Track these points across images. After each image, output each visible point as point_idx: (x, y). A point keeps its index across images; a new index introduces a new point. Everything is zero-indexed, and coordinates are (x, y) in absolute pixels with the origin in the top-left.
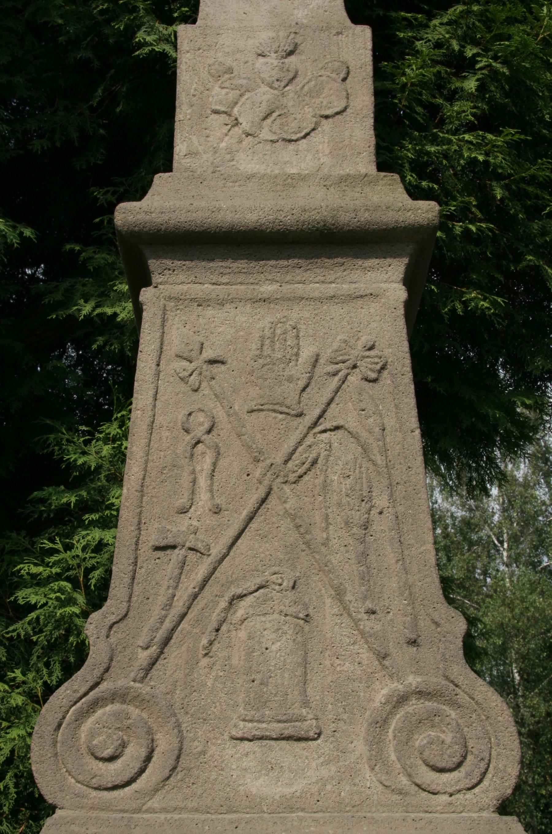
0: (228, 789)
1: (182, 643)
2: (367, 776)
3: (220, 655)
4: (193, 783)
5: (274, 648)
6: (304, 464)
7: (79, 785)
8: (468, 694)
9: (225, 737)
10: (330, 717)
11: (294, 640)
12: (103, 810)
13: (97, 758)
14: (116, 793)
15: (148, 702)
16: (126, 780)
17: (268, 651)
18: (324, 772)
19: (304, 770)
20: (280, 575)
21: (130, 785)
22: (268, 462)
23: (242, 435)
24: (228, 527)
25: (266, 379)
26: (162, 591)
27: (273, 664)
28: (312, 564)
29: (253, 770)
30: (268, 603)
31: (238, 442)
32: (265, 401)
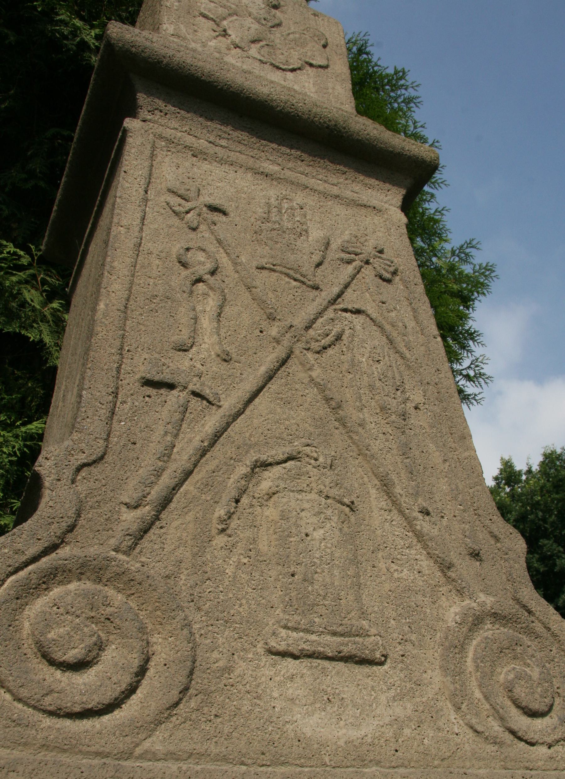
0: (270, 728)
1: (186, 510)
2: (452, 717)
3: (242, 535)
4: (216, 716)
5: (318, 534)
6: (328, 335)
7: (20, 706)
8: (543, 623)
9: (259, 650)
10: (395, 635)
11: (340, 529)
12: (65, 751)
13: (52, 662)
14: (86, 724)
15: (140, 584)
16: (106, 702)
17: (309, 538)
18: (398, 710)
19: (371, 706)
20: (314, 448)
21: (112, 711)
22: (288, 323)
23: (253, 287)
24: (241, 381)
25: (277, 242)
26: (156, 436)
27: (317, 556)
28: (349, 446)
29: (304, 702)
30: (303, 478)
31: (247, 294)
32: (278, 262)
